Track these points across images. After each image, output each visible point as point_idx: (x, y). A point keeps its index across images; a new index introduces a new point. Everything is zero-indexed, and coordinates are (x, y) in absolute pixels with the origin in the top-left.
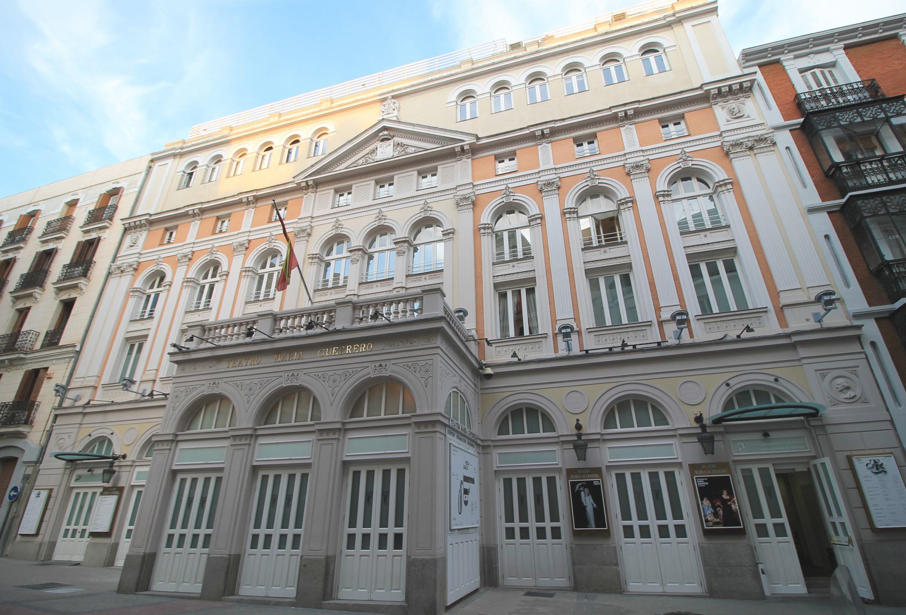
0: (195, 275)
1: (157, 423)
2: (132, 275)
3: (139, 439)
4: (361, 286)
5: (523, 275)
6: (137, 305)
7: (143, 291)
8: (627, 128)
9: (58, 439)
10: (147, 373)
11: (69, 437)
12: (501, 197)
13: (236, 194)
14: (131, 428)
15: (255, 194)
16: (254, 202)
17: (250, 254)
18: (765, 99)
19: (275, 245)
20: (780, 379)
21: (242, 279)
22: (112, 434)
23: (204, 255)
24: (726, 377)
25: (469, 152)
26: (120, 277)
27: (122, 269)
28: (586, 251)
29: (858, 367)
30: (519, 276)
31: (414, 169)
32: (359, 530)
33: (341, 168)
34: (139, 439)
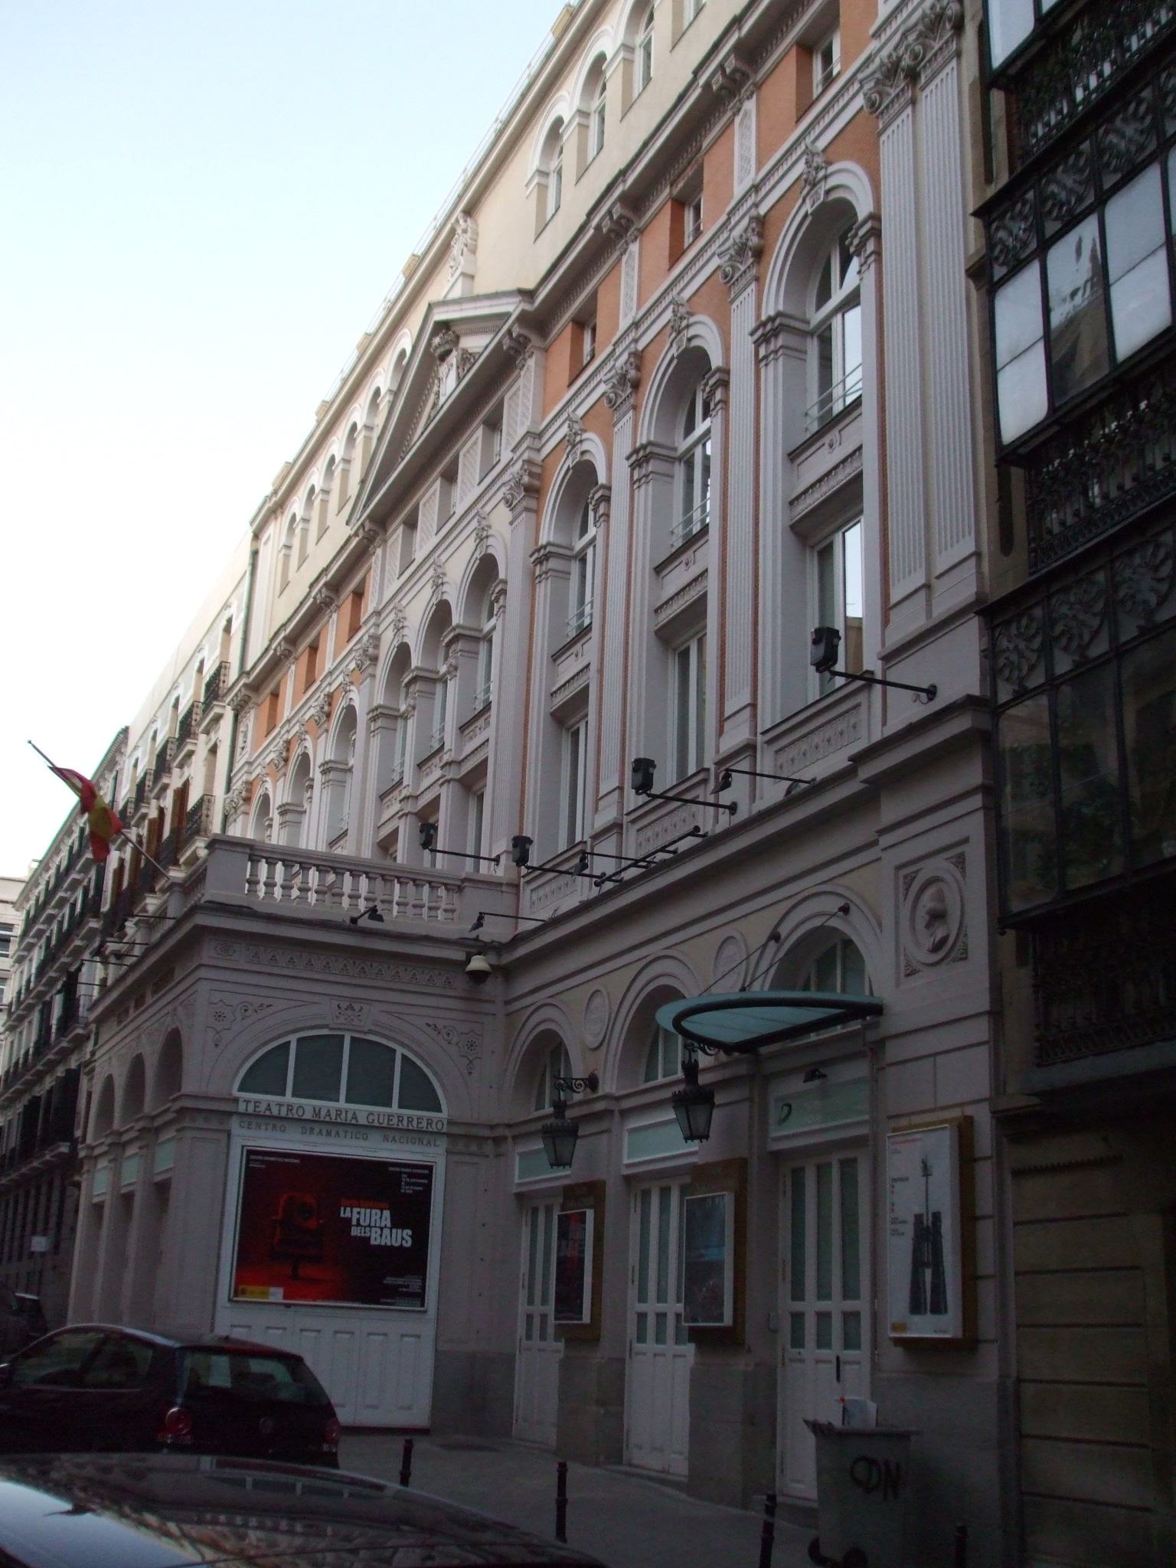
0: (555, 533)
1: (644, 962)
2: (527, 509)
3: (616, 1017)
4: (467, 732)
5: (681, 602)
6: (793, 389)
7: (473, 633)
8: (424, 505)
9: (916, 886)
10: (602, 804)
11: (960, 861)
12: (800, 201)
13: (691, 76)
14: (592, 996)
15: (282, 635)
16: (291, 648)
17: (766, 273)
18: (774, 70)
19: (828, 186)
20: (854, 914)
21: (636, 492)
22: (845, 910)
23: (796, 201)
24: (770, 918)
25: (526, 338)
26: (913, 102)
27: (906, 61)
28: (695, 548)
29: (966, 841)
30: (687, 598)
31: (474, 425)
32: (811, 1305)
33: (419, 435)
34: (616, 1017)
